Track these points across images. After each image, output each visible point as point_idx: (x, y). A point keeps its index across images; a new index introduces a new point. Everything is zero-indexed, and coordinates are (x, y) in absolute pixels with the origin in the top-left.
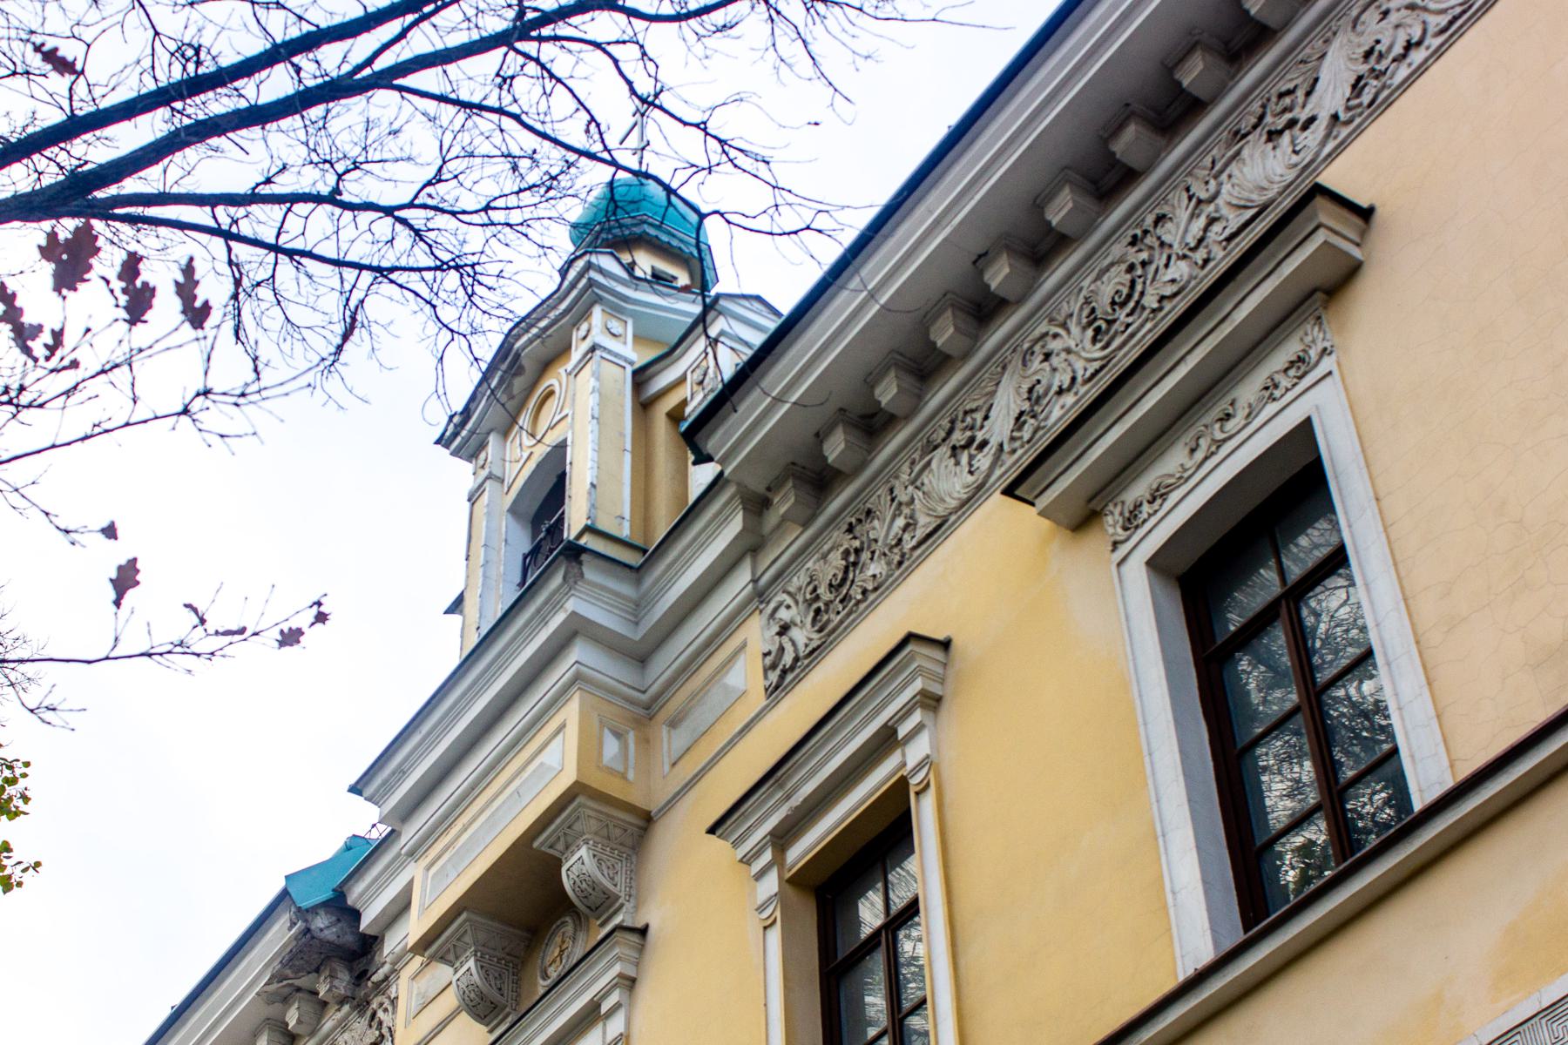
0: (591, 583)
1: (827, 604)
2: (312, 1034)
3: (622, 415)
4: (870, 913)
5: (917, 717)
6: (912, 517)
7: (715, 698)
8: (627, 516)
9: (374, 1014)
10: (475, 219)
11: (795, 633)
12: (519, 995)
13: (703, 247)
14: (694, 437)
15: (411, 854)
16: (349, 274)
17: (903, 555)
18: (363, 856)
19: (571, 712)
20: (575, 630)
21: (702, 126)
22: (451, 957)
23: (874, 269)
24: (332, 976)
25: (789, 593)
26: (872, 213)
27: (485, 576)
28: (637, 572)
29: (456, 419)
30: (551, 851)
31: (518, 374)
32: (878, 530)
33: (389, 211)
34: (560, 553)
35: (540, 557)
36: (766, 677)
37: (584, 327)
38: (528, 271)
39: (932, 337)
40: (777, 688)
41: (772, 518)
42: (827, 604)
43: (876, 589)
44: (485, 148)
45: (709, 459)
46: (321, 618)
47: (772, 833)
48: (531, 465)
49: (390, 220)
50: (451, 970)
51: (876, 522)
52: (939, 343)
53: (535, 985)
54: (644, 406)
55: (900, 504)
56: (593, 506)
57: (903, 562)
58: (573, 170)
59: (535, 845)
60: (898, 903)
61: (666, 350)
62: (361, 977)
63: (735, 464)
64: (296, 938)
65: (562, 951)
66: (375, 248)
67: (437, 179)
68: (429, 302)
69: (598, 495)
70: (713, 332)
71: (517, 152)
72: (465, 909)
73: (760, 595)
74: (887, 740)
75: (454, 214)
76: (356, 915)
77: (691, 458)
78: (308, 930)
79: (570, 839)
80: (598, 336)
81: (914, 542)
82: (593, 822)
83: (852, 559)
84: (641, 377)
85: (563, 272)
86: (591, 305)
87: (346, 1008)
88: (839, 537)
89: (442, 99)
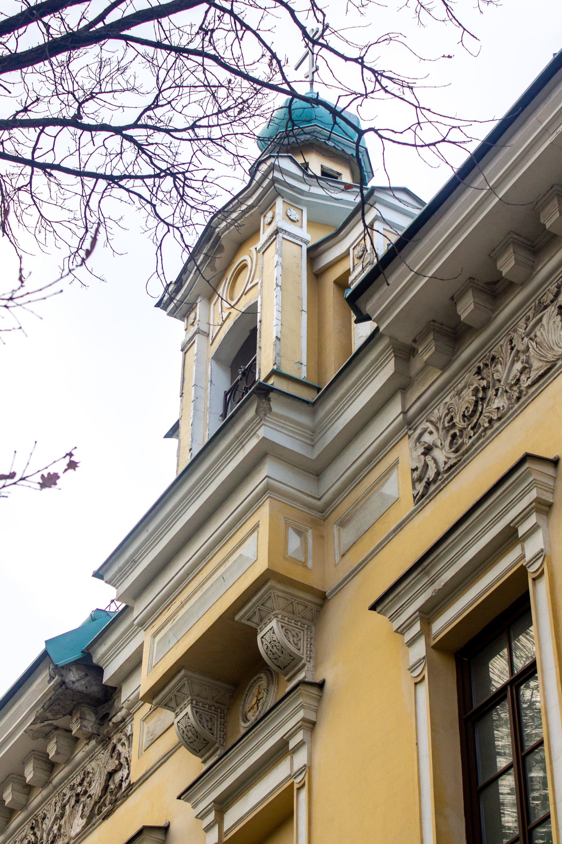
0: (277, 415)
1: (461, 431)
2: (67, 762)
3: (299, 283)
4: (498, 671)
5: (533, 520)
6: (527, 362)
7: (374, 506)
8: (305, 362)
9: (114, 747)
10: (184, 135)
11: (436, 453)
12: (225, 734)
13: (361, 149)
14: (356, 301)
15: (142, 624)
16: (90, 182)
17: (521, 392)
18: (104, 625)
19: (263, 515)
20: (265, 452)
21: (360, 61)
22: (173, 704)
23: (494, 169)
24: (82, 718)
25: (431, 422)
26: (490, 127)
27: (195, 409)
28: (312, 406)
29: (171, 288)
30: (249, 623)
31: (219, 251)
32: (502, 373)
33: (118, 131)
34: (253, 392)
35: (238, 395)
36: (414, 488)
37: (270, 215)
38: (224, 176)
39: (542, 221)
40: (423, 496)
41: (418, 363)
42: (461, 431)
43: (499, 419)
44: (191, 80)
45: (368, 318)
46: (72, 465)
47: (420, 610)
48: (230, 323)
49: (118, 138)
50: (173, 714)
51: (499, 367)
52: (548, 226)
53: (238, 725)
54: (316, 275)
55: (518, 352)
56: (278, 355)
57: (521, 398)
58: (259, 96)
59: (237, 618)
60: (520, 664)
61: (332, 232)
62: (104, 718)
63: (388, 321)
64: (54, 688)
65: (258, 700)
66: (108, 160)
67: (155, 105)
68: (150, 203)
69: (281, 347)
70: (368, 219)
71: (214, 82)
72: (183, 667)
73: (409, 423)
74: (509, 538)
75: (168, 131)
76: (100, 671)
77: (354, 318)
78: (63, 683)
79: (263, 614)
80: (280, 222)
81: (529, 382)
82: (281, 600)
83: (480, 395)
84: (314, 253)
85: (253, 172)
86: (275, 198)
87: (93, 742)
88: (470, 377)
89: (158, 45)
